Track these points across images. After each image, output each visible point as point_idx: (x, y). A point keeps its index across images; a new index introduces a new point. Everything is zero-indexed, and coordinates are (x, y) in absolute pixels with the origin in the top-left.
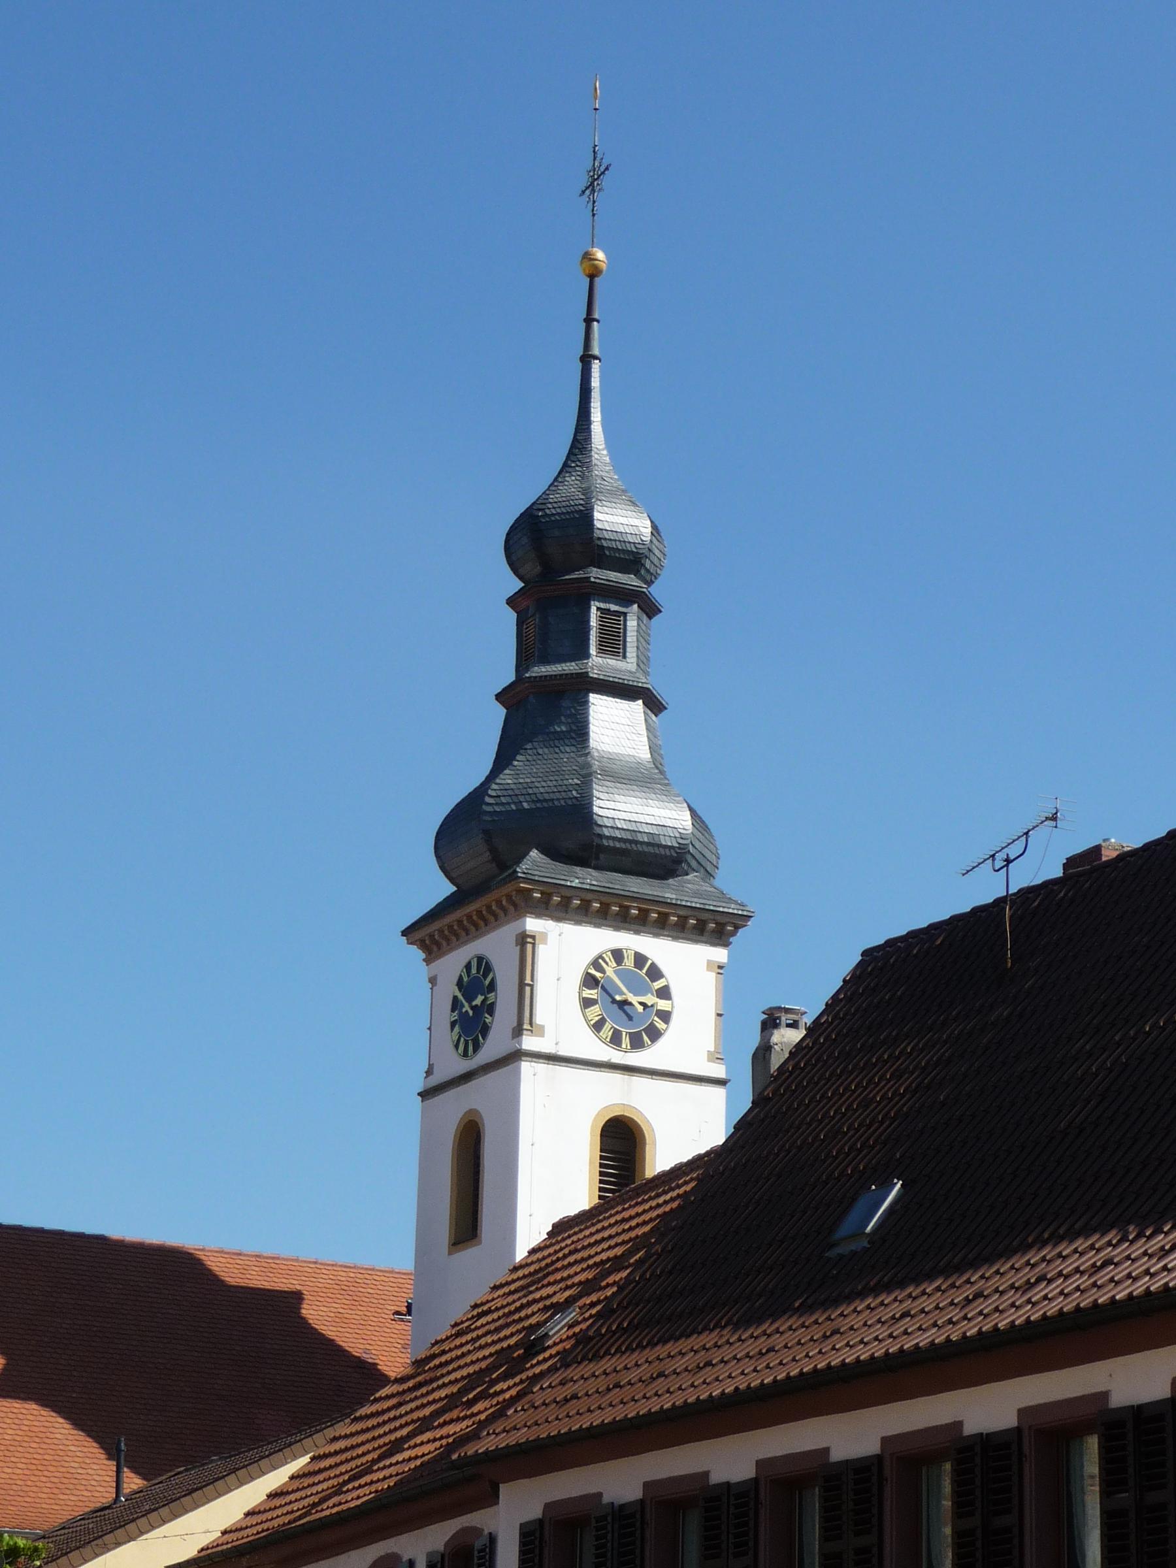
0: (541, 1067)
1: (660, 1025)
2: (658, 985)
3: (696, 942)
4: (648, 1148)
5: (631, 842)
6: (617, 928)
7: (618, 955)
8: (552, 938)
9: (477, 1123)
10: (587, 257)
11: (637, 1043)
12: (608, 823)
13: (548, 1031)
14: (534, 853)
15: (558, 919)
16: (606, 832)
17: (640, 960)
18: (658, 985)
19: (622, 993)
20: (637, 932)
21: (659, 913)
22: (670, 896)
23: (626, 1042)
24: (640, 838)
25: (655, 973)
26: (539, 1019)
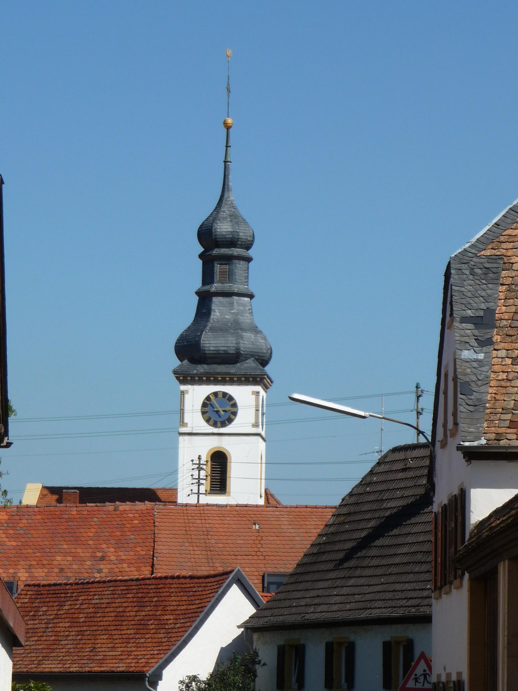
0: (187, 438)
1: (232, 417)
2: (232, 403)
3: (247, 385)
4: (228, 464)
5: (217, 354)
6: (215, 385)
7: (216, 394)
8: (190, 392)
9: (225, 494)
10: (225, 123)
11: (223, 424)
12: (208, 349)
13: (189, 425)
14: (186, 360)
15: (192, 385)
16: (207, 352)
17: (225, 394)
18: (232, 403)
19: (217, 408)
20: (223, 385)
21: (229, 378)
22: (233, 371)
23: (219, 424)
24: (220, 352)
25: (231, 398)
26: (14, 408)
